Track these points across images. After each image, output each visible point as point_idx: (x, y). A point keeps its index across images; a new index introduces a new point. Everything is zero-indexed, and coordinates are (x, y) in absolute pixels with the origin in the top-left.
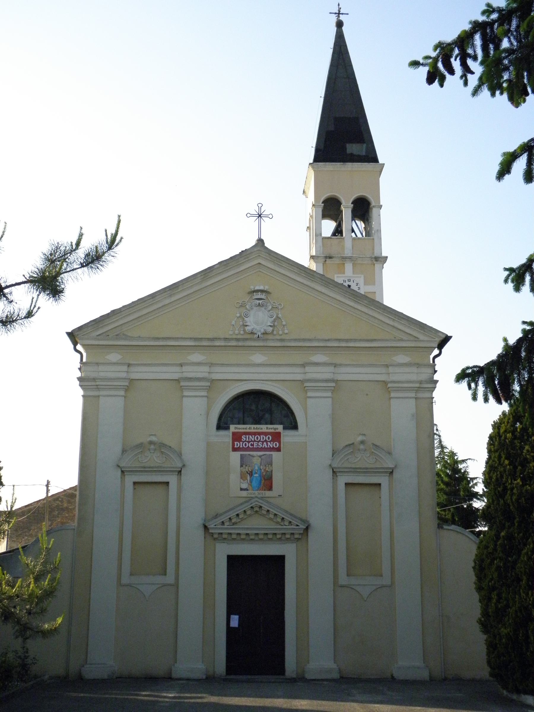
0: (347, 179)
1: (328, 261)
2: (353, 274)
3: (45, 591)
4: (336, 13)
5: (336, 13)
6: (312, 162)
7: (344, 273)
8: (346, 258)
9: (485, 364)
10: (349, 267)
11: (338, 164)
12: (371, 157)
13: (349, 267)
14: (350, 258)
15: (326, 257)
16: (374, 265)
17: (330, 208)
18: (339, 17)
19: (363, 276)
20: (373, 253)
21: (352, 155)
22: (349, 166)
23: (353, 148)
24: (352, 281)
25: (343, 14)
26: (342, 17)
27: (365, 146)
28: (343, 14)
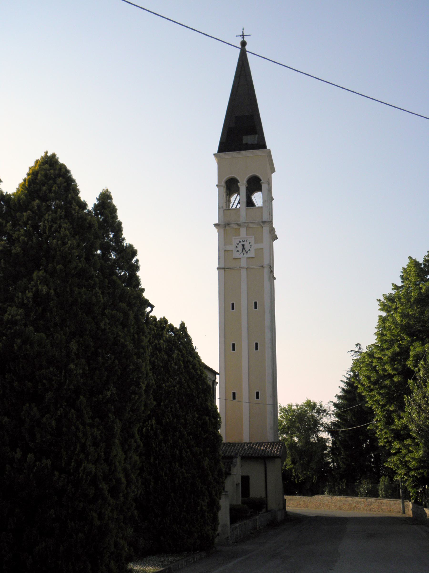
0: (244, 164)
1: (228, 227)
2: (247, 235)
3: (384, 417)
4: (241, 36)
5: (241, 36)
6: (216, 152)
7: (239, 235)
8: (240, 224)
9: (128, 255)
10: (243, 230)
11: (235, 153)
12: (261, 145)
13: (243, 230)
14: (243, 224)
15: (225, 224)
16: (262, 227)
17: (230, 186)
18: (243, 38)
19: (254, 236)
20: (262, 218)
21: (247, 144)
22: (244, 153)
23: (248, 139)
24: (245, 241)
25: (246, 36)
26: (246, 39)
27: (257, 136)
28: (246, 36)
